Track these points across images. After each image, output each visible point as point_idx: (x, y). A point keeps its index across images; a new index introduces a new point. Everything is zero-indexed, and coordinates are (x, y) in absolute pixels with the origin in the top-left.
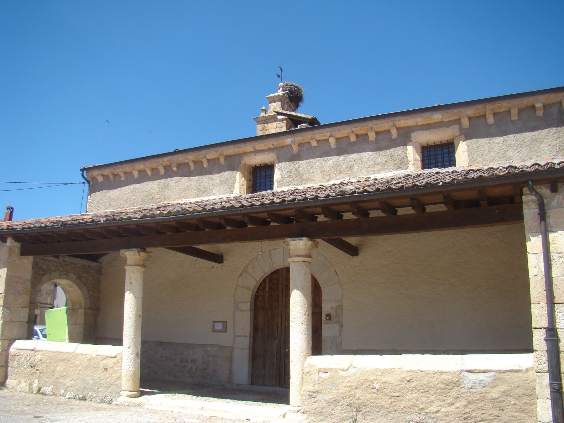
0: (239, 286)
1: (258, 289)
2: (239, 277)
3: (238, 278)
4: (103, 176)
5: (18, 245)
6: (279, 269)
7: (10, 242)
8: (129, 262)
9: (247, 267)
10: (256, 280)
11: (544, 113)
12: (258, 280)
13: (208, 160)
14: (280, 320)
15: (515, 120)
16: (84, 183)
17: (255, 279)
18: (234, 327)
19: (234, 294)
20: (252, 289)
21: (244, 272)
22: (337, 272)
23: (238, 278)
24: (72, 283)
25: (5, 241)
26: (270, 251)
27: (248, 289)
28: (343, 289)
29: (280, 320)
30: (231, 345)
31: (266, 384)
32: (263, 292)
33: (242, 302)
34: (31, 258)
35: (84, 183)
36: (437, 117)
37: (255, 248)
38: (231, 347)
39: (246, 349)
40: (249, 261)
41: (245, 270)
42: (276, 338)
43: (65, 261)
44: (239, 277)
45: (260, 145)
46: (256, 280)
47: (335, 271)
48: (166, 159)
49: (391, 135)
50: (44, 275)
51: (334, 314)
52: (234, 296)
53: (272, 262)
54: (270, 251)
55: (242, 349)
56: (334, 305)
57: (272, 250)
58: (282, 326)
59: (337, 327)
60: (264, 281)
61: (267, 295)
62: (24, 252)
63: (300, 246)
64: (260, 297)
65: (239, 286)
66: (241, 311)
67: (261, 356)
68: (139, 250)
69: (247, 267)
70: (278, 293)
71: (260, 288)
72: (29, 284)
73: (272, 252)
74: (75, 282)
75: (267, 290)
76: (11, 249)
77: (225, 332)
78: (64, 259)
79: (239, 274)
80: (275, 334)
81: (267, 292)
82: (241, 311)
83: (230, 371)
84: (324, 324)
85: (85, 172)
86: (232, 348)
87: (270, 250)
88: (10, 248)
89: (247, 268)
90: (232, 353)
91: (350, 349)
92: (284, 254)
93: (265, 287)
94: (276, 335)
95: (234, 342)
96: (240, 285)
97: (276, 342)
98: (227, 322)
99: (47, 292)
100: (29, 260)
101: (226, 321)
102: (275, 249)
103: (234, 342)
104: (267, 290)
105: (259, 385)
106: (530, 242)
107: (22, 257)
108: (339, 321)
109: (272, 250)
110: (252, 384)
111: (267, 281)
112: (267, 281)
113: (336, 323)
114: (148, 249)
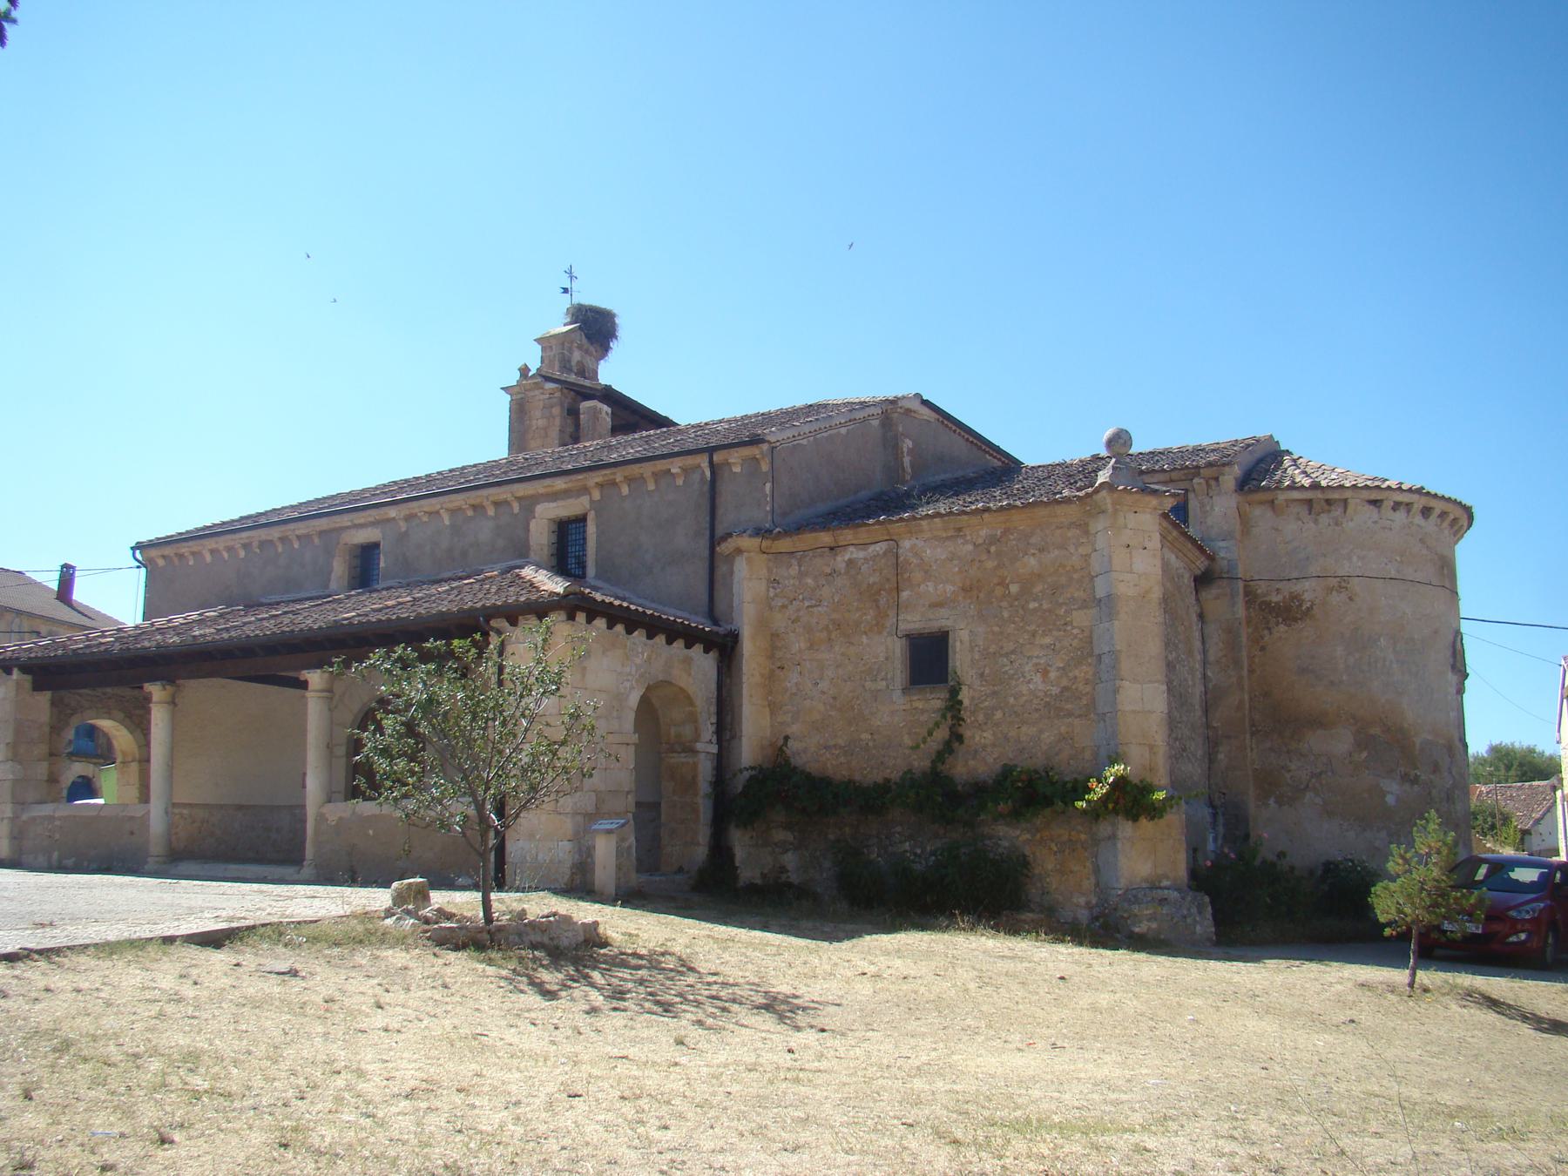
4: (164, 557)
5: (29, 678)
7: (16, 674)
8: (155, 698)
11: (684, 481)
13: (298, 537)
15: (652, 491)
16: (138, 567)
24: (116, 724)
25: (8, 671)
34: (48, 694)
35: (138, 567)
36: (560, 484)
43: (104, 694)
45: (360, 518)
48: (245, 535)
49: (512, 508)
50: (72, 714)
62: (38, 687)
63: (871, 580)
68: (164, 682)
72: (47, 729)
74: (122, 722)
76: (18, 684)
78: (576, 588)
85: (138, 552)
88: (18, 683)
99: (1271, 634)
100: (44, 698)
106: (644, 639)
107: (35, 693)
114: (178, 682)
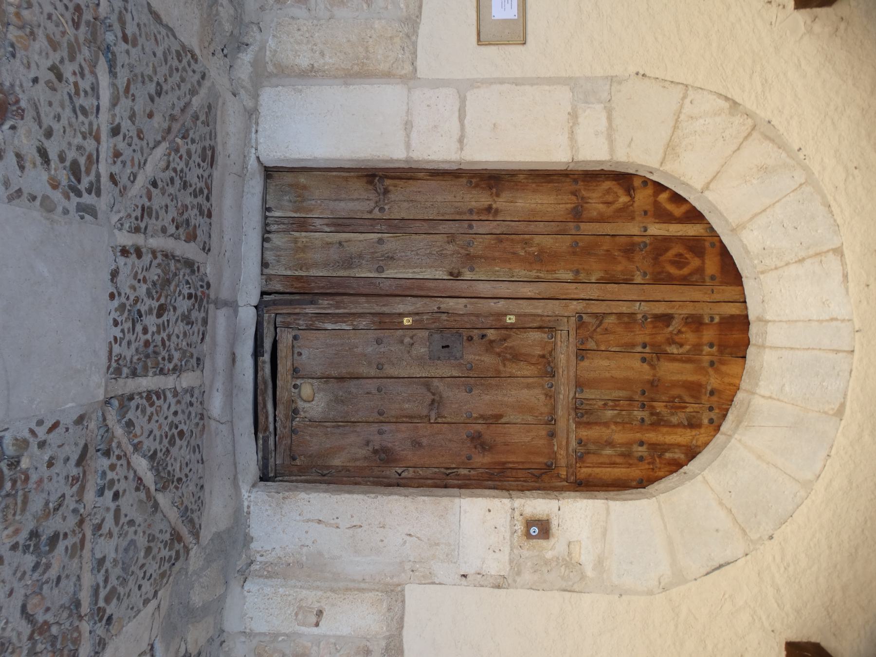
0: (684, 97)
1: (660, 188)
2: (727, 99)
3: (720, 95)
6: (741, 284)
9: (773, 138)
10: (707, 187)
12: (707, 194)
14: (527, 290)
17: (711, 181)
18: (502, 82)
19: (648, 74)
20: (668, 167)
21: (750, 122)
22: (723, 569)
23: (720, 95)
26: (839, 252)
27: (671, 148)
28: (650, 593)
29: (527, 290)
30: (423, 71)
31: (269, 232)
32: (646, 212)
33: (610, 119)
37: (856, 172)
38: (415, 70)
39: (408, 146)
40: (796, 148)
41: (754, 128)
42: (455, 275)
44: (727, 99)
46: (707, 187)
47: (728, 564)
51: (549, 555)
52: (637, 74)
53: (787, 264)
54: (839, 252)
55: (408, 126)
56: (586, 557)
57: (843, 264)
58: (502, 302)
59: (497, 565)
60: (695, 216)
61: (632, 229)
64: (624, 199)
65: (684, 97)
66: (574, 116)
67: (382, 210)
69: (773, 138)
70: (638, 279)
71: (663, 197)
73: (833, 262)
75: (656, 229)
77: (479, 40)
79: (738, 100)
80: (472, 270)
81: (646, 230)
82: (574, 116)
83: (309, 74)
84: (509, 505)
86: (410, 79)
87: (842, 255)
89: (767, 138)
90: (388, 76)
91: (406, 619)
92: (820, 321)
93: (664, 217)
94: (468, 275)
95: (437, 84)
96: (687, 101)
97: (440, 274)
98: (521, 48)
101: (530, 38)
102: (845, 276)
103: (437, 84)
104: (656, 229)
105: (264, 200)
108: (519, 573)
109: (843, 264)
110: (269, 172)
111: (691, 230)
112: (691, 230)
113: (511, 561)
